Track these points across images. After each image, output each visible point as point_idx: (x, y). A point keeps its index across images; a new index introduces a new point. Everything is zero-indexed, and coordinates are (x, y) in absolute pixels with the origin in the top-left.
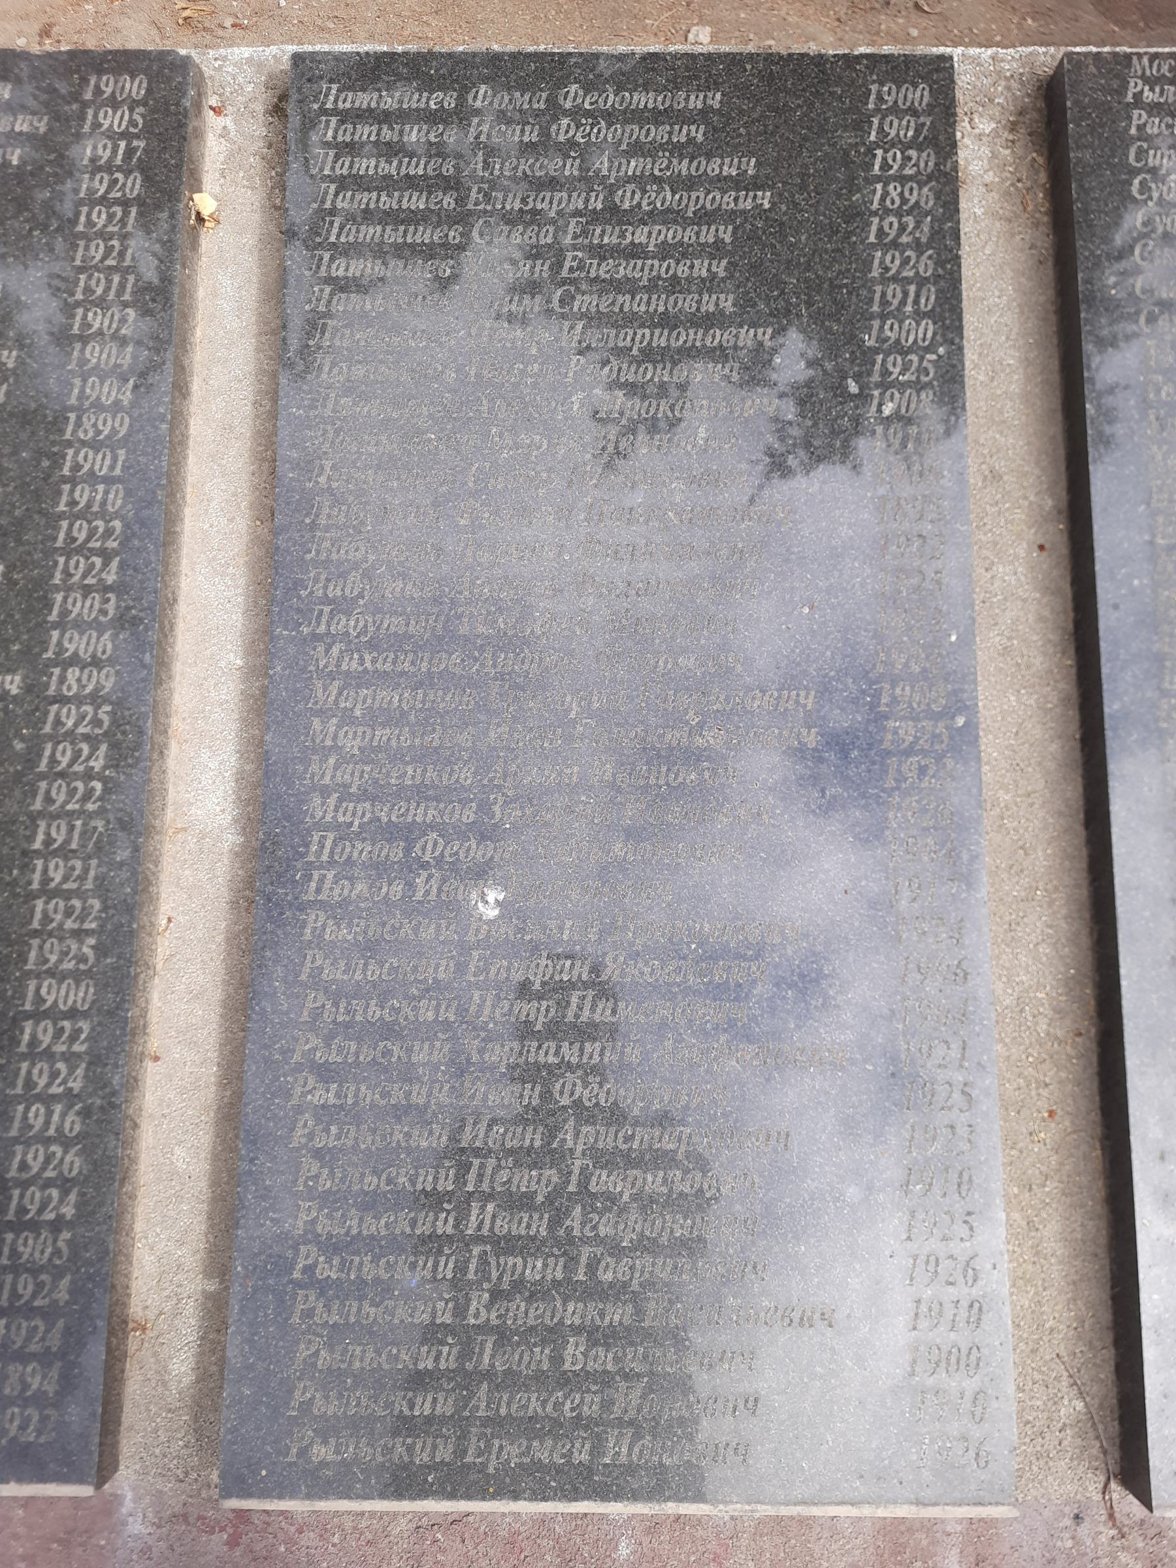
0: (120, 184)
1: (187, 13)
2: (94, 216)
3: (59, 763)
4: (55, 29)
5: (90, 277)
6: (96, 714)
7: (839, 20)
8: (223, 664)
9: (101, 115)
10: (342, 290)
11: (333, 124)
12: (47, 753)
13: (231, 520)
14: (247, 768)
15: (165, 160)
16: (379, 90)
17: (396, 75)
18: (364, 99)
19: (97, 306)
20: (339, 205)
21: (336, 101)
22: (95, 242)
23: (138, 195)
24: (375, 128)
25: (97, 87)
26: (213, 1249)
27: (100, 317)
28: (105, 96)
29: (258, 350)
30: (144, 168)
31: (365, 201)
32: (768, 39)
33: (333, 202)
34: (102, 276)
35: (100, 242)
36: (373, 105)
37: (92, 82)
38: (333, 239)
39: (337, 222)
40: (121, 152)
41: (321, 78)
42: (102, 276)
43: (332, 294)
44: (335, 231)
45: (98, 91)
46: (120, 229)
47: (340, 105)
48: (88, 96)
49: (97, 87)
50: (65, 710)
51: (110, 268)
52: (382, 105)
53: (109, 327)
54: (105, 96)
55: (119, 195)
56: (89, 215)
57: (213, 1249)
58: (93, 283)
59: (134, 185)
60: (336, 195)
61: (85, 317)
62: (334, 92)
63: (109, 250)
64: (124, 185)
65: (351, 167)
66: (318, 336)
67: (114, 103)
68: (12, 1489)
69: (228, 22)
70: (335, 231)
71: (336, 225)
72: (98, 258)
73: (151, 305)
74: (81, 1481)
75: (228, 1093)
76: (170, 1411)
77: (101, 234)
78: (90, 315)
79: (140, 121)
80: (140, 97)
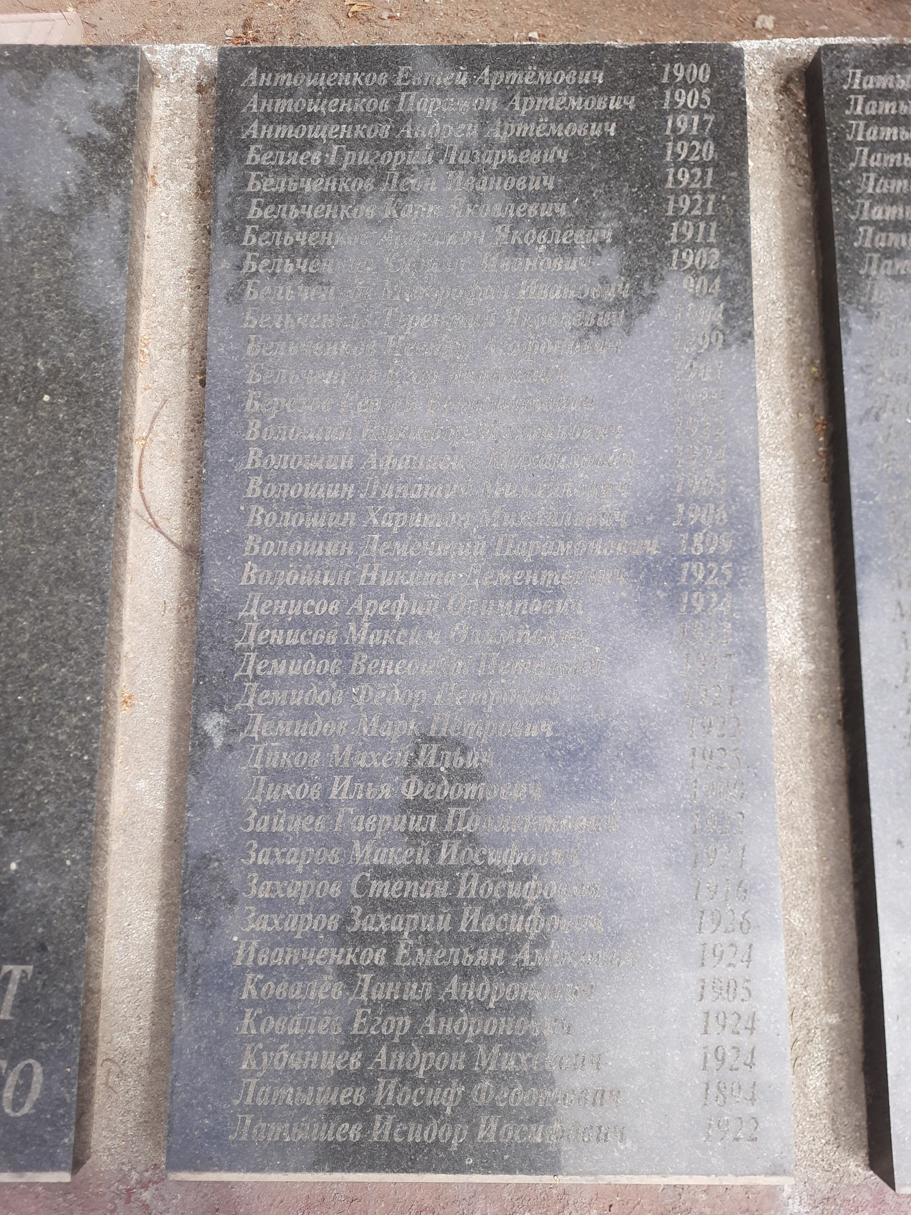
0: (697, 150)
1: (354, 8)
2: (679, 176)
3: (695, 608)
4: (253, 22)
5: (681, 225)
6: (720, 569)
7: (868, 9)
8: (780, 527)
9: (677, 95)
10: (882, 230)
11: (860, 101)
12: (685, 600)
13: (778, 413)
14: (810, 609)
15: (732, 130)
16: (894, 74)
17: (905, 62)
18: (883, 81)
19: (689, 247)
20: (872, 164)
21: (861, 84)
22: (683, 196)
23: (713, 158)
24: (894, 104)
25: (671, 73)
26: (831, 990)
27: (692, 256)
28: (678, 80)
29: (787, 278)
30: (717, 139)
31: (892, 160)
32: (821, 25)
33: (868, 162)
34: (690, 223)
35: (686, 196)
36: (891, 86)
37: (667, 69)
38: (870, 190)
39: (872, 176)
40: (695, 124)
41: (847, 64)
42: (690, 223)
43: (874, 234)
44: (872, 183)
45: (672, 76)
46: (701, 186)
47: (865, 86)
48: (665, 80)
49: (671, 73)
50: (695, 566)
51: (696, 217)
52: (898, 85)
53: (700, 263)
54: (678, 80)
55: (697, 158)
56: (675, 174)
57: (831, 990)
58: (684, 229)
59: (708, 150)
60: (869, 156)
61: (680, 256)
62: (858, 76)
63: (694, 203)
64: (701, 150)
65: (878, 134)
66: (866, 266)
67: (686, 85)
68: (6, 1177)
69: (385, 15)
70: (872, 183)
71: (872, 180)
72: (686, 209)
73: (731, 245)
74: (54, 1166)
75: (828, 868)
76: (811, 1116)
77: (686, 190)
78: (684, 254)
79: (708, 100)
80: (706, 81)
